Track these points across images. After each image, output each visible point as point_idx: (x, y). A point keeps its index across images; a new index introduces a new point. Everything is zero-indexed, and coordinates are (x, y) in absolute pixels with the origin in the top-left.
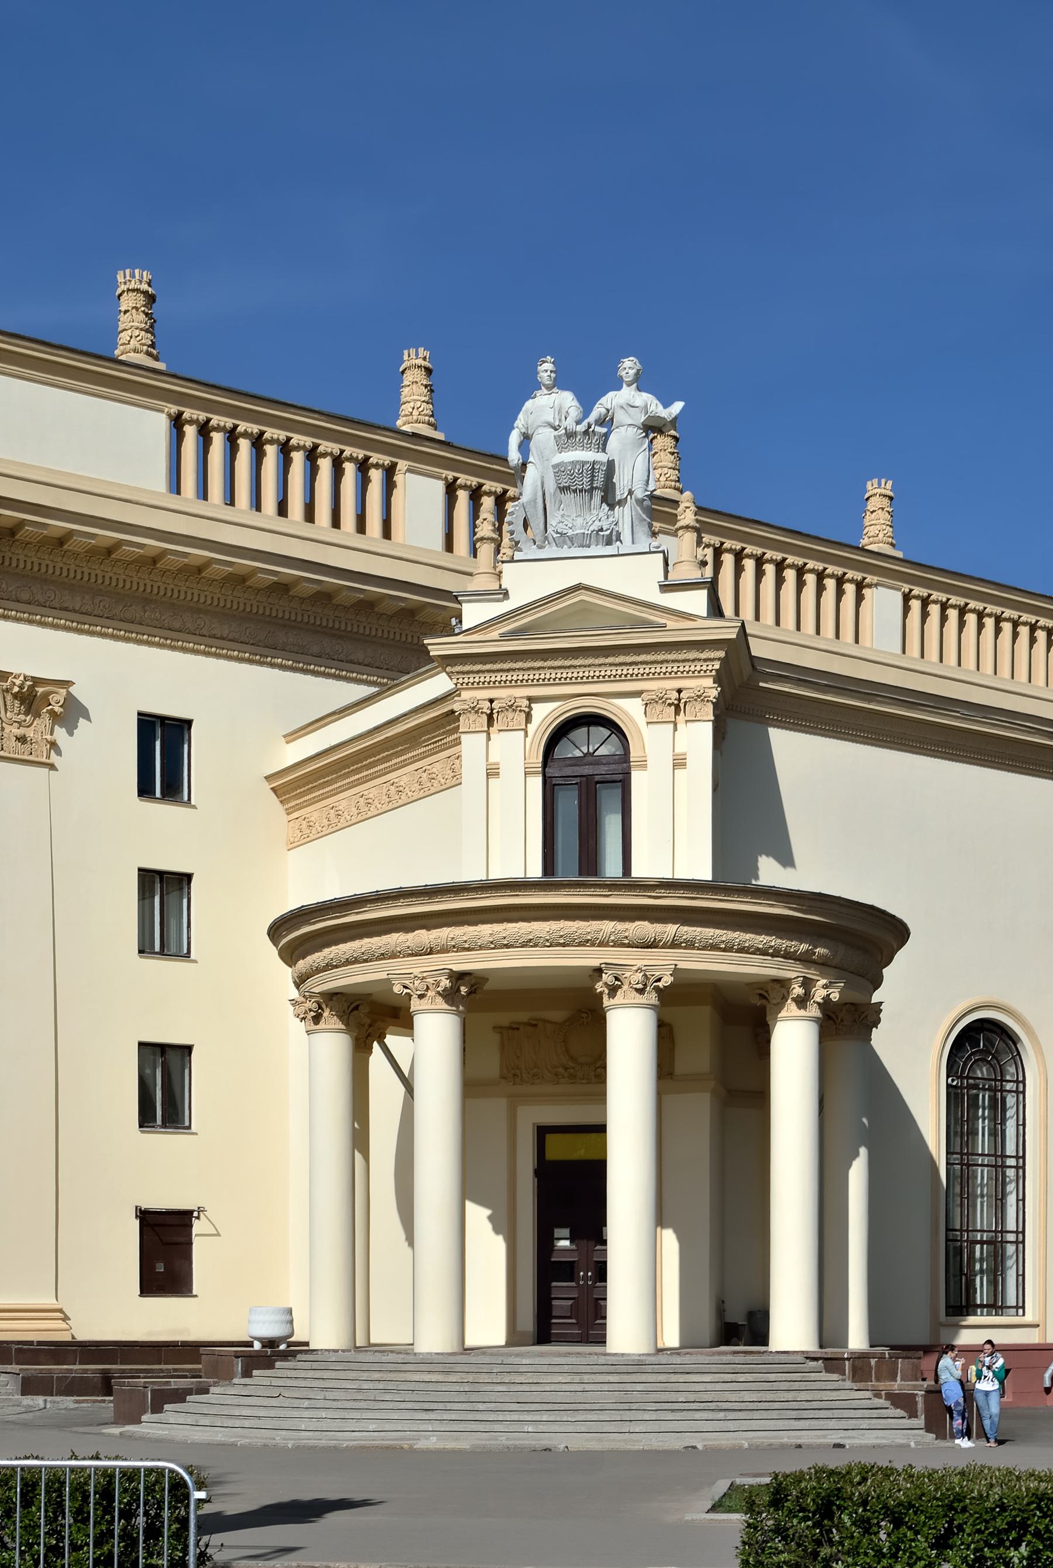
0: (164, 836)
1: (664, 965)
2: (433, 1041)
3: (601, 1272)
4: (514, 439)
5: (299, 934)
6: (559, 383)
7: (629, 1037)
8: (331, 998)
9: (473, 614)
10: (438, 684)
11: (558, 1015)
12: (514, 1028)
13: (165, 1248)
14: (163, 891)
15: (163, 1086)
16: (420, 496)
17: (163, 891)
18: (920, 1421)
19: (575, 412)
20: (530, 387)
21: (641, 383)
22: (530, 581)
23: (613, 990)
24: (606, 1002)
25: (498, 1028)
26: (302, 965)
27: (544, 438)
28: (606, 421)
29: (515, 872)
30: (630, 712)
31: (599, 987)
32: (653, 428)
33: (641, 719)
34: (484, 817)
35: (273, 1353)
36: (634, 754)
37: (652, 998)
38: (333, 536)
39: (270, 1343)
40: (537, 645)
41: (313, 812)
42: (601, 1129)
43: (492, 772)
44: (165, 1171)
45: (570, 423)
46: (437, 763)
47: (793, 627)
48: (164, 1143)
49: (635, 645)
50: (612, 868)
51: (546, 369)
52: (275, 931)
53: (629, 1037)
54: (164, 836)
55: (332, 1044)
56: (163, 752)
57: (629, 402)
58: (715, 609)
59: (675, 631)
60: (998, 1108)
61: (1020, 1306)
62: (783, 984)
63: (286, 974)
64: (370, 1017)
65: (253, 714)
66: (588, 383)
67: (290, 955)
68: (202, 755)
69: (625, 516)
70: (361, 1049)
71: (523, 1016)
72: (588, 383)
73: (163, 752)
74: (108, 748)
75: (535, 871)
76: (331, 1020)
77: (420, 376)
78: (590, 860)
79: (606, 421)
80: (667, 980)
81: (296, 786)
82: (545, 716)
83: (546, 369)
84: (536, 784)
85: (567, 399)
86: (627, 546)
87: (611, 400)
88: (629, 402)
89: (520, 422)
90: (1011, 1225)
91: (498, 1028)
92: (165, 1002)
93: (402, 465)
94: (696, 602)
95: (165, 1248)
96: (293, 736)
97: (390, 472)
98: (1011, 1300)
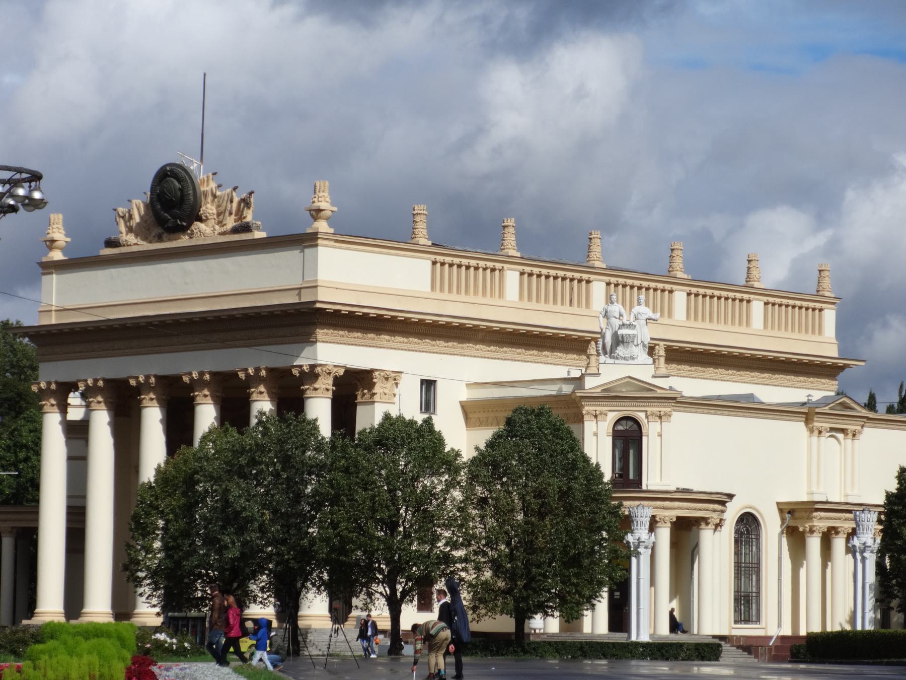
1: (674, 514)
30: (641, 416)
61: (758, 620)
62: (705, 520)
82: (612, 417)
98: (754, 619)
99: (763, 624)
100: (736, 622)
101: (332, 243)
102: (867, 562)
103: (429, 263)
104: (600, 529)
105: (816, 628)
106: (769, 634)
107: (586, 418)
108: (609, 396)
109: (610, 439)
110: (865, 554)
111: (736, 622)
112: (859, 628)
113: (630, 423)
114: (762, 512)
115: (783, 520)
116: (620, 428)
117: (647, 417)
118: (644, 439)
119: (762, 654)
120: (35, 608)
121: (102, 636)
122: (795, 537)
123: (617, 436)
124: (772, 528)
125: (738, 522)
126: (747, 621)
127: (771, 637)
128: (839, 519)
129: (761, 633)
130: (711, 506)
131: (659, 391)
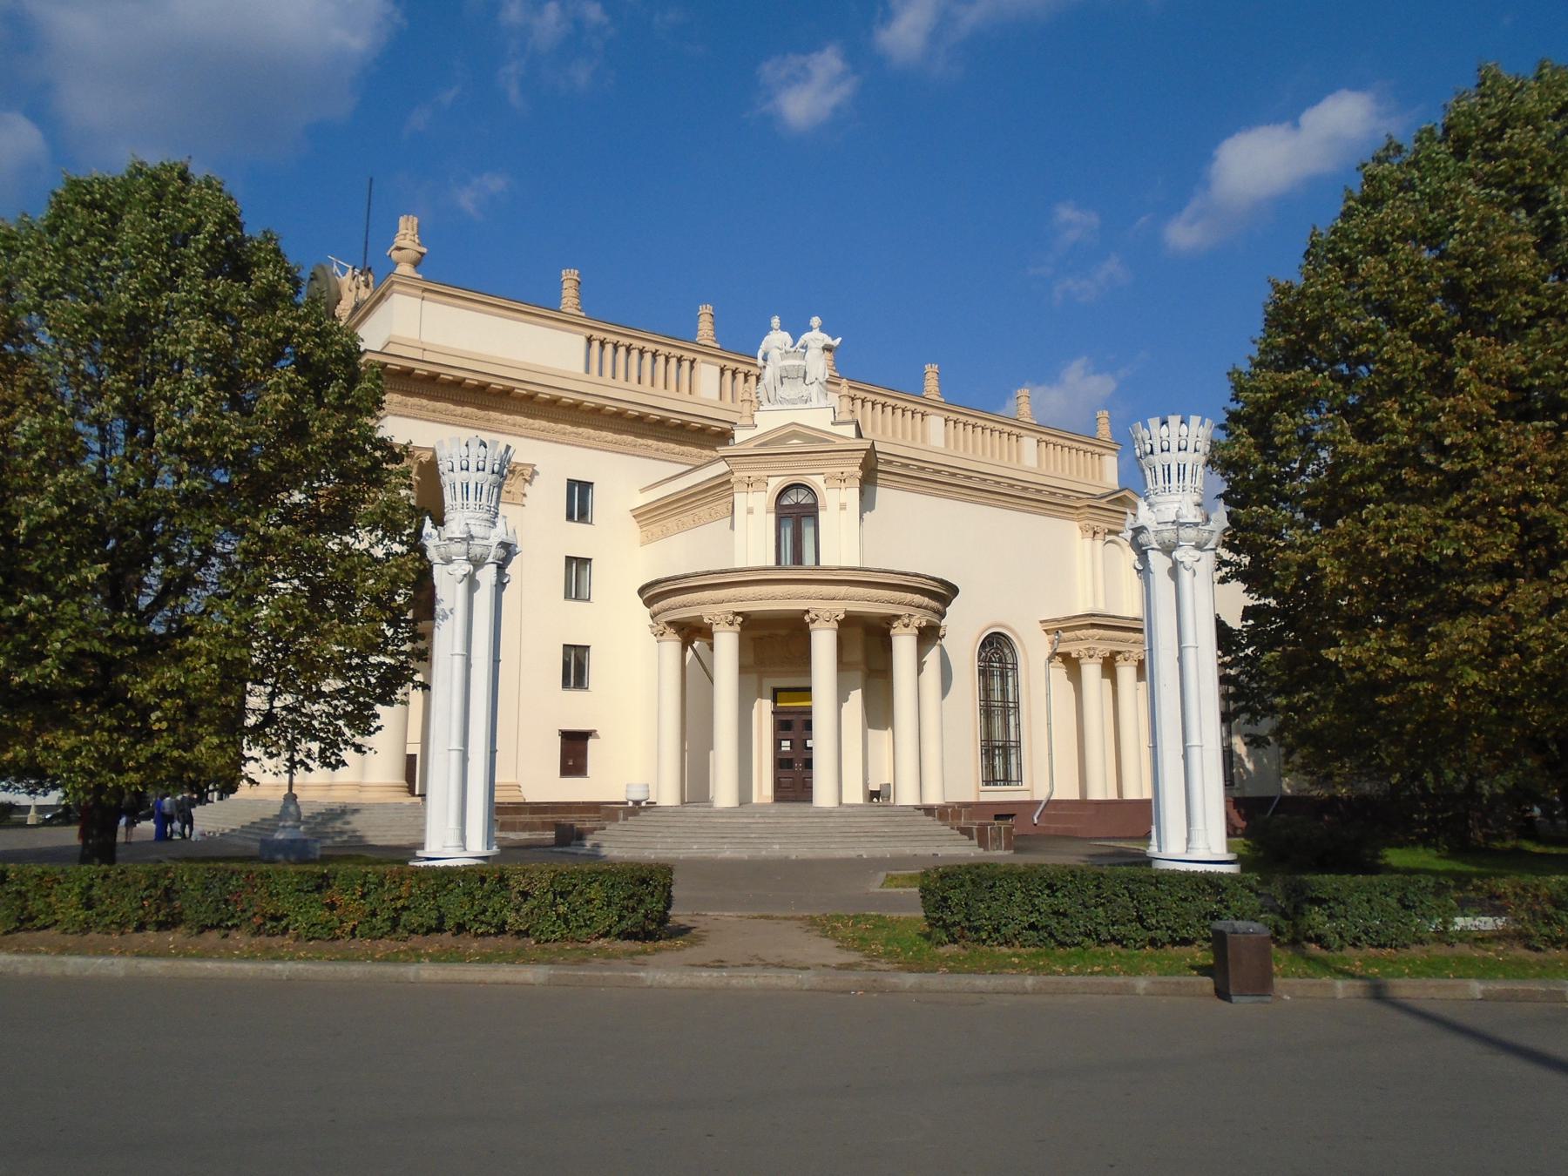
0: (578, 539)
1: (840, 609)
2: (726, 645)
3: (808, 764)
4: (760, 354)
5: (652, 594)
6: (783, 328)
7: (824, 645)
8: (670, 623)
9: (740, 435)
10: (721, 468)
11: (783, 632)
12: (761, 639)
13: (574, 750)
14: (577, 566)
15: (576, 667)
16: (707, 374)
17: (577, 566)
18: (975, 842)
19: (790, 341)
20: (768, 329)
21: (823, 329)
22: (769, 420)
23: (813, 621)
24: (811, 626)
25: (754, 639)
26: (656, 607)
27: (775, 354)
28: (805, 347)
29: (762, 564)
30: (817, 482)
31: (807, 618)
32: (827, 348)
33: (823, 486)
34: (751, 538)
35: (637, 809)
36: (820, 504)
37: (836, 625)
38: (665, 393)
39: (637, 803)
40: (774, 448)
41: (655, 528)
42: (809, 689)
43: (750, 511)
44: (576, 711)
45: (788, 348)
46: (721, 507)
47: (894, 433)
48: (575, 695)
49: (814, 446)
50: (809, 559)
51: (776, 321)
52: (641, 591)
53: (824, 645)
54: (578, 539)
55: (672, 645)
56: (579, 500)
57: (816, 338)
58: (859, 435)
59: (840, 444)
60: (1004, 677)
61: (1019, 781)
62: (898, 617)
63: (647, 611)
64: (692, 632)
65: (626, 476)
66: (797, 329)
67: (648, 603)
68: (599, 501)
69: (815, 389)
70: (685, 646)
71: (766, 633)
72: (797, 329)
73: (579, 500)
74: (548, 496)
75: (772, 562)
76: (670, 631)
77: (709, 318)
78: (798, 558)
79: (805, 347)
80: (842, 616)
81: (646, 515)
82: (776, 484)
83: (776, 321)
84: (772, 517)
85: (786, 336)
86: (814, 404)
87: (806, 337)
88: (816, 338)
89: (763, 346)
90: (1012, 738)
91: (754, 639)
92: (578, 623)
93: (699, 358)
94: (850, 431)
95: (574, 750)
96: (643, 490)
97: (692, 362)
98: (1014, 777)
102: (1186, 576)
103: (582, 341)
105: (1067, 791)
110: (1177, 554)
111: (987, 783)
114: (1017, 630)
119: (994, 840)
121: (1232, 775)
124: (1033, 652)
125: (983, 645)
126: (1007, 780)
127: (1039, 803)
128: (1126, 641)
129: (1025, 797)
130: (909, 597)
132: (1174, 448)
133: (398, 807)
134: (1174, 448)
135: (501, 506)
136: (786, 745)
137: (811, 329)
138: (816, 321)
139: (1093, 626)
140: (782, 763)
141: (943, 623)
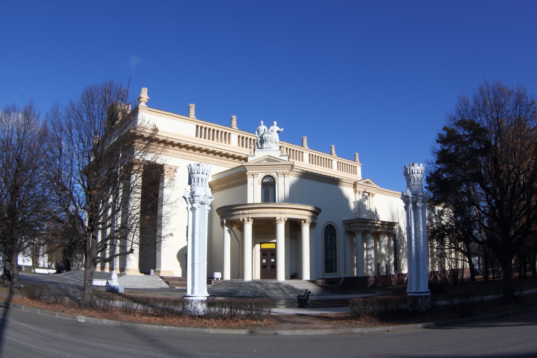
2: (248, 228)
7: (281, 229)
9: (250, 159)
21: (277, 125)
30: (274, 175)
53: (281, 229)
59: (283, 162)
61: (336, 271)
66: (269, 125)
82: (261, 175)
83: (262, 122)
87: (272, 128)
98: (334, 270)
99: (338, 273)
100: (326, 272)
101: (215, 163)
104: (97, 171)
106: (341, 276)
107: (248, 176)
108: (258, 165)
109: (260, 186)
111: (326, 272)
112: (430, 294)
113: (270, 178)
115: (346, 228)
116: (265, 181)
117: (277, 174)
118: (276, 185)
120: (125, 267)
122: (351, 234)
123: (264, 185)
127: (342, 278)
129: (337, 276)
131: (282, 162)
132: (201, 173)
133: (137, 276)
134: (201, 173)
135: (248, 202)
136: (264, 261)
137: (273, 125)
138: (275, 123)
139: (360, 222)
140: (263, 266)
141: (316, 221)
